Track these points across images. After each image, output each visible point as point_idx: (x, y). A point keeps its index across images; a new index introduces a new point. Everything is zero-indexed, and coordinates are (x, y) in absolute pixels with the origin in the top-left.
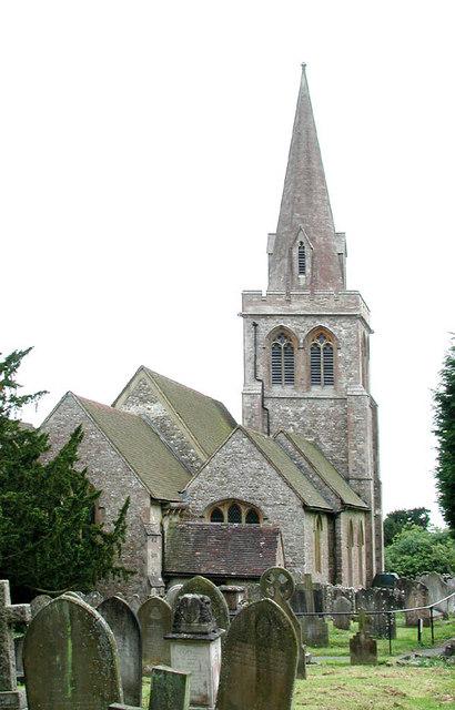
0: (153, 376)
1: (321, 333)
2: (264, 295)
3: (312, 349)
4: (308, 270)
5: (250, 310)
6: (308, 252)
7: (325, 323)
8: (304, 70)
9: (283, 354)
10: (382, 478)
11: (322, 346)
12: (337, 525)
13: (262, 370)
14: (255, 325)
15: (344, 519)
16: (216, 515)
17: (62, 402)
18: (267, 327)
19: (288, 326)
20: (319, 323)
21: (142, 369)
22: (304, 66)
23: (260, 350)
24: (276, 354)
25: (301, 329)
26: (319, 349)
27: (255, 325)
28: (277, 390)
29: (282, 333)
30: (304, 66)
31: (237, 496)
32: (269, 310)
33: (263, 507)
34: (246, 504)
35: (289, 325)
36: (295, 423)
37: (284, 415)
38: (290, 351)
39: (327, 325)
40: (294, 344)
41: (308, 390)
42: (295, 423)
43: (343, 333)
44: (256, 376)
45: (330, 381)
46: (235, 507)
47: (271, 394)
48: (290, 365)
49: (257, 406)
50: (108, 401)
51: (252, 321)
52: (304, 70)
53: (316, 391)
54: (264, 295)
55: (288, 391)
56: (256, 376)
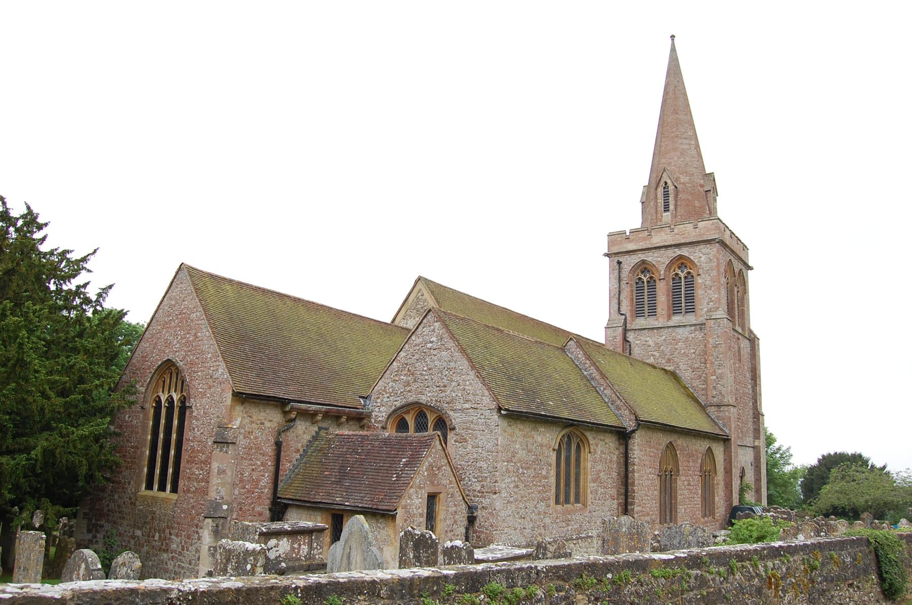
0: (437, 290)
1: (681, 262)
2: (628, 234)
3: (673, 279)
4: (672, 207)
5: (615, 249)
6: (671, 188)
7: (685, 252)
8: (673, 40)
9: (646, 288)
10: (413, 284)
11: (682, 275)
12: (630, 447)
13: (625, 308)
14: (619, 263)
15: (638, 442)
16: (402, 425)
17: (175, 277)
18: (629, 262)
19: (649, 259)
20: (678, 252)
21: (419, 279)
22: (673, 37)
23: (623, 286)
24: (640, 289)
25: (660, 260)
26: (680, 278)
27: (619, 263)
28: (641, 322)
29: (644, 267)
30: (673, 37)
31: (423, 399)
32: (631, 247)
33: (451, 413)
34: (432, 409)
35: (650, 257)
36: (655, 353)
37: (646, 345)
38: (652, 282)
39: (686, 254)
40: (655, 277)
41: (669, 318)
42: (655, 353)
43: (702, 259)
44: (619, 310)
45: (691, 310)
46: (420, 411)
47: (633, 327)
48: (653, 296)
49: (619, 339)
50: (389, 321)
51: (615, 256)
52: (673, 40)
53: (676, 319)
54: (628, 234)
55: (651, 322)
56: (619, 310)
